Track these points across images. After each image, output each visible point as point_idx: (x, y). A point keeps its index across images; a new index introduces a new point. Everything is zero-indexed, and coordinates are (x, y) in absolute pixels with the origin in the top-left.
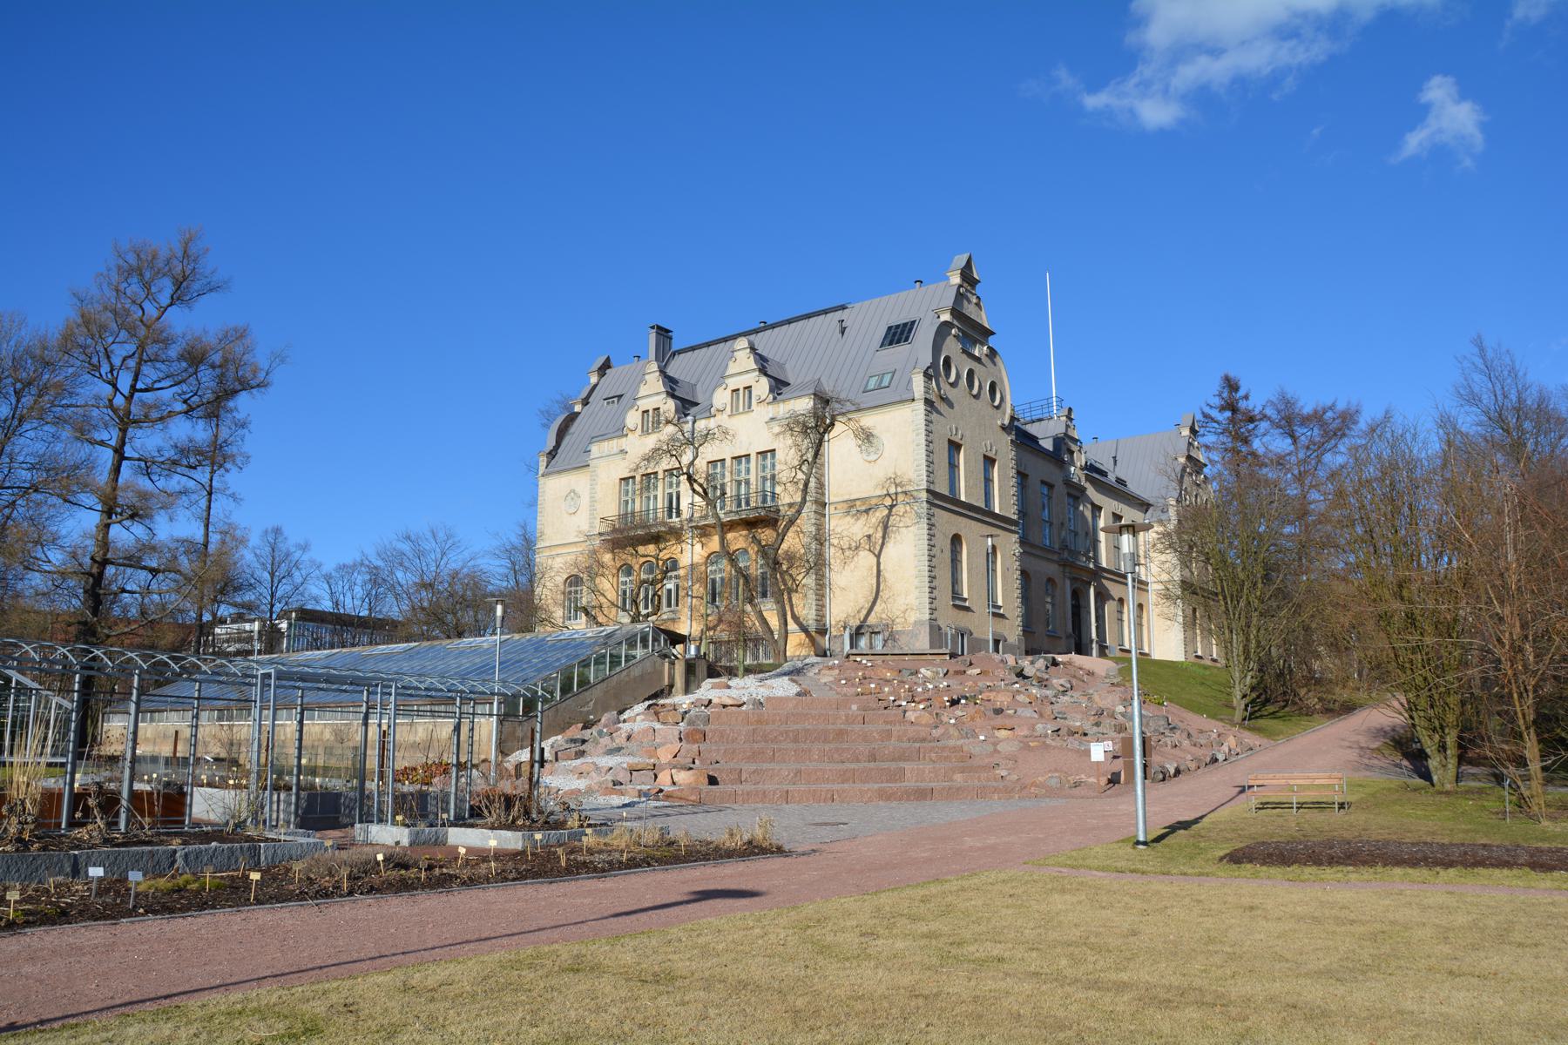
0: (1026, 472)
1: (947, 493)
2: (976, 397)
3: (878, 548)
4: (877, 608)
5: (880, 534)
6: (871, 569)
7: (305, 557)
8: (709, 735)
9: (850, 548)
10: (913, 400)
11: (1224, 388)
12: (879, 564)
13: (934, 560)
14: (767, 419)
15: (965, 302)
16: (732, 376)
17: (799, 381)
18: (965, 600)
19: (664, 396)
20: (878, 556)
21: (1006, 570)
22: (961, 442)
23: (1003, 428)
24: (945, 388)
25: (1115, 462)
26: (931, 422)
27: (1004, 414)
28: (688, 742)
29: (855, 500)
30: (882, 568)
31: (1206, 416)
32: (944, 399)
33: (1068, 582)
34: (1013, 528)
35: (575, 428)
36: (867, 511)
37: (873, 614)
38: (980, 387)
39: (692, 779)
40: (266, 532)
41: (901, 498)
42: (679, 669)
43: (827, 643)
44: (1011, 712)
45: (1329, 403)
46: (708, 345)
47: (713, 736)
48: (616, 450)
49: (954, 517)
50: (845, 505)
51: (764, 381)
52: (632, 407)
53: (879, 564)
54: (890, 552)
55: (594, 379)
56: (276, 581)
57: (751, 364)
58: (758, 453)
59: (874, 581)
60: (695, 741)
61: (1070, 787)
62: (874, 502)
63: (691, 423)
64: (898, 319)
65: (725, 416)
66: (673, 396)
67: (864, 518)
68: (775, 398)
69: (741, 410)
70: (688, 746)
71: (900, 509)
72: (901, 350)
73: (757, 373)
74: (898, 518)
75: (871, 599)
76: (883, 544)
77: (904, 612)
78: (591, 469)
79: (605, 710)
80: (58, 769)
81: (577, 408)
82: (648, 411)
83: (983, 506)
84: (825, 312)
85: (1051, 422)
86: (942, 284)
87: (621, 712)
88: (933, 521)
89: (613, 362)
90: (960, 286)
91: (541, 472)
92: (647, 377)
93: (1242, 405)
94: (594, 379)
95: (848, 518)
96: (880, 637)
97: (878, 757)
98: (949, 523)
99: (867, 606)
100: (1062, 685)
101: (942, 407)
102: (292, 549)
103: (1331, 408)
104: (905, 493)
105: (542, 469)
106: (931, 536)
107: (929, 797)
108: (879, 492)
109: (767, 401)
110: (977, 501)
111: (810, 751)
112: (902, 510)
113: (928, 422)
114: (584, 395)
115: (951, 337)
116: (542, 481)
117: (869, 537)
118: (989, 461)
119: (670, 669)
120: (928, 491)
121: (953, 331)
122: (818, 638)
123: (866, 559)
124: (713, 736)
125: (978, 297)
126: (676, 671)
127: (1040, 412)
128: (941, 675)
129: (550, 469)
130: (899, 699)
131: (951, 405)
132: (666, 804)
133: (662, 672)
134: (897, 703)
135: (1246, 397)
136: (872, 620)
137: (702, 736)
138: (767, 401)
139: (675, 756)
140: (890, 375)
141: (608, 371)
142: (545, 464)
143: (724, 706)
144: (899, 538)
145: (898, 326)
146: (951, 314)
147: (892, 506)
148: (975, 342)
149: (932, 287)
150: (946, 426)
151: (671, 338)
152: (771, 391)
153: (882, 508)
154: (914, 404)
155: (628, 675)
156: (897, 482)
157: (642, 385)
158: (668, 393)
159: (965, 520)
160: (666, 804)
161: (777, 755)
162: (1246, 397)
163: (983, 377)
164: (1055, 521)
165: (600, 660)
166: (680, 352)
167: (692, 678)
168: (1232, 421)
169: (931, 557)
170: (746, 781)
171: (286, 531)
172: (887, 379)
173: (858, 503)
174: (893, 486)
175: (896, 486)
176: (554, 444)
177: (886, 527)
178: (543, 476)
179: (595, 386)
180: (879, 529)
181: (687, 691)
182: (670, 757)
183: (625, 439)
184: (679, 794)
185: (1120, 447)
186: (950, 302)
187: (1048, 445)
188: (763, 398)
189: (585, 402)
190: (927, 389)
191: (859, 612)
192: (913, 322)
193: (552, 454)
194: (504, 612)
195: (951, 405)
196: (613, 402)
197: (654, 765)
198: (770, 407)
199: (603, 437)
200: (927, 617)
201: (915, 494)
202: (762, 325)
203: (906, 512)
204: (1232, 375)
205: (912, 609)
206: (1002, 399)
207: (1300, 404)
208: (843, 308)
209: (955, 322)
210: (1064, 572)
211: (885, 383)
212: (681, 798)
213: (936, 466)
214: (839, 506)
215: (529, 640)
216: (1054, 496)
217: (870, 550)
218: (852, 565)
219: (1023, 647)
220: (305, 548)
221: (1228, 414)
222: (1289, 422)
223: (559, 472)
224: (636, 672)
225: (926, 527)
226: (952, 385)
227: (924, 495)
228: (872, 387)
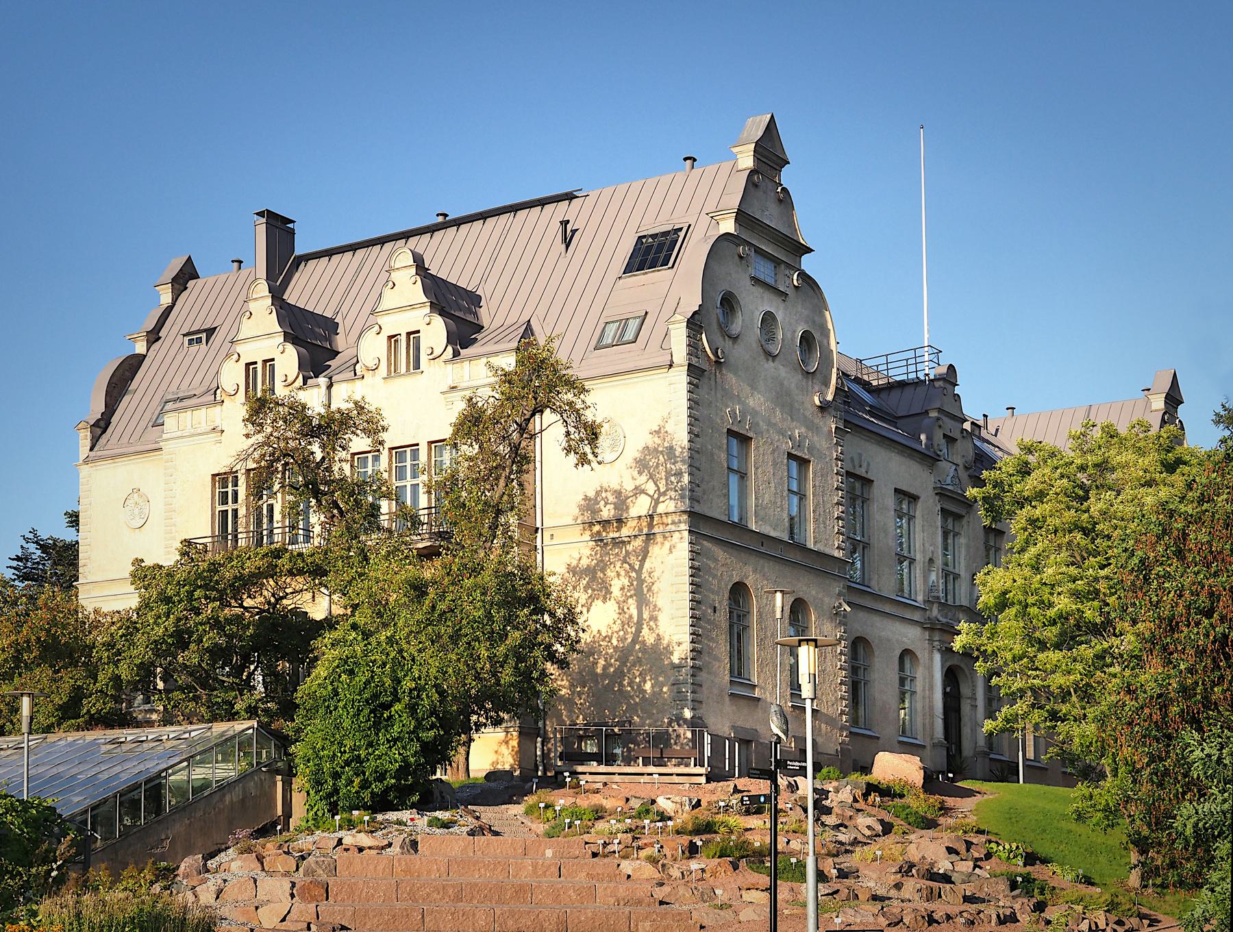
0: (869, 476)
8: (333, 890)
14: (446, 388)
16: (387, 311)
17: (496, 323)
22: (750, 434)
28: (303, 898)
33: (937, 657)
35: (140, 381)
46: (353, 248)
48: (205, 427)
51: (439, 323)
52: (228, 356)
57: (416, 293)
58: (430, 443)
60: (313, 898)
63: (324, 388)
64: (656, 225)
70: (302, 906)
72: (657, 278)
78: (164, 455)
79: (188, 852)
81: (140, 348)
83: (786, 538)
84: (542, 203)
86: (726, 166)
87: (212, 855)
91: (82, 457)
100: (869, 827)
109: (444, 357)
127: (904, 370)
137: (323, 891)
139: (283, 920)
141: (191, 284)
142: (88, 443)
149: (711, 169)
152: (450, 340)
157: (245, 319)
161: (427, 919)
164: (918, 557)
166: (307, 258)
172: (633, 325)
178: (86, 461)
179: (170, 309)
183: (219, 407)
186: (734, 200)
188: (437, 353)
189: (153, 336)
193: (101, 426)
194: (34, 705)
196: (199, 341)
198: (449, 366)
199: (181, 401)
202: (440, 219)
208: (570, 197)
210: (931, 640)
211: (629, 335)
215: (70, 744)
216: (918, 514)
223: (113, 457)
228: (610, 341)
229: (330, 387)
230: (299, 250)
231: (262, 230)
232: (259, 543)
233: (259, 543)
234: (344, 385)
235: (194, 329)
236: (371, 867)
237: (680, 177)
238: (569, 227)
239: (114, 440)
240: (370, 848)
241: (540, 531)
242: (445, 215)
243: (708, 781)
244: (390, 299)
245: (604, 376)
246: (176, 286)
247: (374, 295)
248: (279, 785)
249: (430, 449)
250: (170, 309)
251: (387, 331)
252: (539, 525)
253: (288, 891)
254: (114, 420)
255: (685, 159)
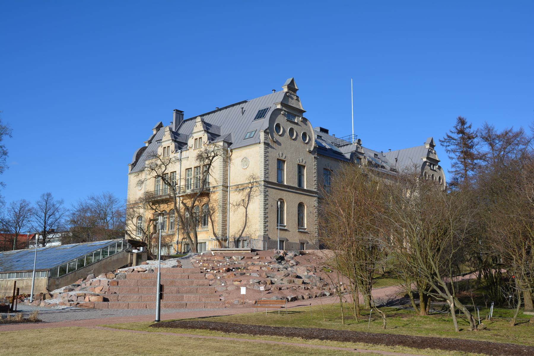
1: (276, 182)
2: (295, 140)
3: (246, 205)
4: (245, 230)
5: (247, 199)
6: (243, 214)
7: (61, 207)
8: (120, 283)
9: (236, 205)
10: (260, 143)
11: (459, 123)
12: (246, 211)
13: (267, 210)
15: (290, 99)
17: (224, 134)
18: (285, 226)
19: (171, 141)
20: (246, 208)
21: (309, 213)
22: (284, 160)
23: (310, 152)
24: (276, 137)
25: (397, 161)
26: (268, 152)
27: (311, 146)
28: (111, 285)
29: (239, 185)
30: (247, 213)
31: (449, 137)
32: (277, 142)
34: (314, 195)
36: (243, 189)
37: (244, 232)
38: (297, 135)
39: (97, 299)
40: (44, 195)
41: (255, 184)
42: (135, 257)
43: (227, 244)
44: (248, 274)
45: (509, 129)
47: (121, 283)
49: (279, 191)
50: (235, 187)
53: (246, 211)
54: (250, 206)
55: (155, 132)
56: (47, 216)
59: (245, 219)
61: (240, 304)
62: (245, 185)
63: (180, 153)
65: (192, 150)
66: (208, 132)
67: (242, 192)
68: (210, 142)
69: (198, 147)
71: (254, 189)
72: (261, 120)
73: (204, 132)
74: (253, 193)
75: (243, 226)
76: (248, 203)
77: (255, 232)
80: (340, 301)
81: (147, 145)
82: (197, 139)
85: (352, 146)
88: (267, 193)
89: (164, 124)
90: (287, 93)
91: (129, 173)
92: (165, 133)
93: (467, 131)
94: (155, 132)
95: (236, 192)
96: (246, 242)
97: (180, 292)
98: (276, 195)
99: (242, 229)
101: (275, 145)
102: (55, 203)
103: (510, 131)
104: (256, 182)
105: (129, 171)
106: (266, 200)
107: (185, 307)
108: (247, 182)
109: (207, 144)
110: (294, 184)
111: (153, 289)
112: (255, 189)
113: (266, 152)
114: (150, 139)
115: (281, 115)
116: (129, 176)
117: (243, 200)
118: (301, 168)
119: (131, 257)
120: (264, 181)
121: (282, 113)
122: (223, 242)
123: (242, 209)
124: (121, 283)
125: (297, 97)
126: (134, 258)
128: (240, 259)
129: (132, 171)
130: (208, 269)
131: (279, 144)
132: (79, 308)
133: (127, 258)
134: (207, 271)
135: (470, 127)
136: (243, 235)
137: (117, 283)
138: (207, 144)
139: (101, 291)
140: (254, 132)
142: (131, 169)
143: (139, 272)
144: (253, 201)
145: (262, 110)
146: (281, 105)
147: (252, 187)
148: (295, 116)
149: (279, 92)
150: (275, 154)
151: (183, 115)
152: (208, 139)
153: (248, 188)
154: (260, 145)
155: (111, 259)
156: (254, 177)
157: (163, 137)
158: (173, 140)
159: (285, 192)
160: (79, 308)
161: (139, 290)
162: (470, 127)
163: (299, 130)
165: (97, 254)
167: (140, 260)
168: (462, 138)
169: (265, 209)
170: (120, 300)
171: (53, 195)
173: (240, 186)
174: (252, 179)
175: (253, 179)
176: (135, 160)
177: (249, 196)
178: (130, 174)
179: (155, 135)
180: (247, 197)
181: (137, 264)
182: (99, 291)
184: (86, 305)
185: (400, 153)
187: (348, 156)
189: (150, 142)
190: (266, 138)
191: (239, 232)
192: (268, 108)
193: (134, 165)
195: (279, 144)
197: (85, 294)
200: (262, 234)
201: (260, 182)
202: (217, 109)
203: (256, 190)
204: (462, 117)
205: (258, 230)
206: (310, 139)
207: (495, 130)
208: (246, 102)
209: (284, 109)
212: (86, 306)
213: (270, 171)
214: (233, 187)
217: (243, 206)
218: (237, 212)
219: (318, 245)
220: (61, 202)
221: (461, 135)
222: (489, 139)
224: (114, 258)
225: (263, 196)
226: (280, 135)
227: (263, 183)
229: (181, 153)
230: (185, 118)
231: (174, 114)
232: (197, 187)
233: (197, 187)
234: (185, 152)
235: (157, 140)
236: (136, 276)
237: (271, 95)
238: (244, 110)
239: (137, 168)
240: (141, 271)
241: (229, 187)
242: (218, 108)
243: (251, 252)
244: (195, 130)
245: (247, 146)
246: (157, 129)
247: (161, 137)
248: (129, 255)
249: (194, 169)
250: (155, 135)
251: (195, 138)
252: (229, 185)
253: (107, 283)
254: (137, 163)
255: (273, 90)
